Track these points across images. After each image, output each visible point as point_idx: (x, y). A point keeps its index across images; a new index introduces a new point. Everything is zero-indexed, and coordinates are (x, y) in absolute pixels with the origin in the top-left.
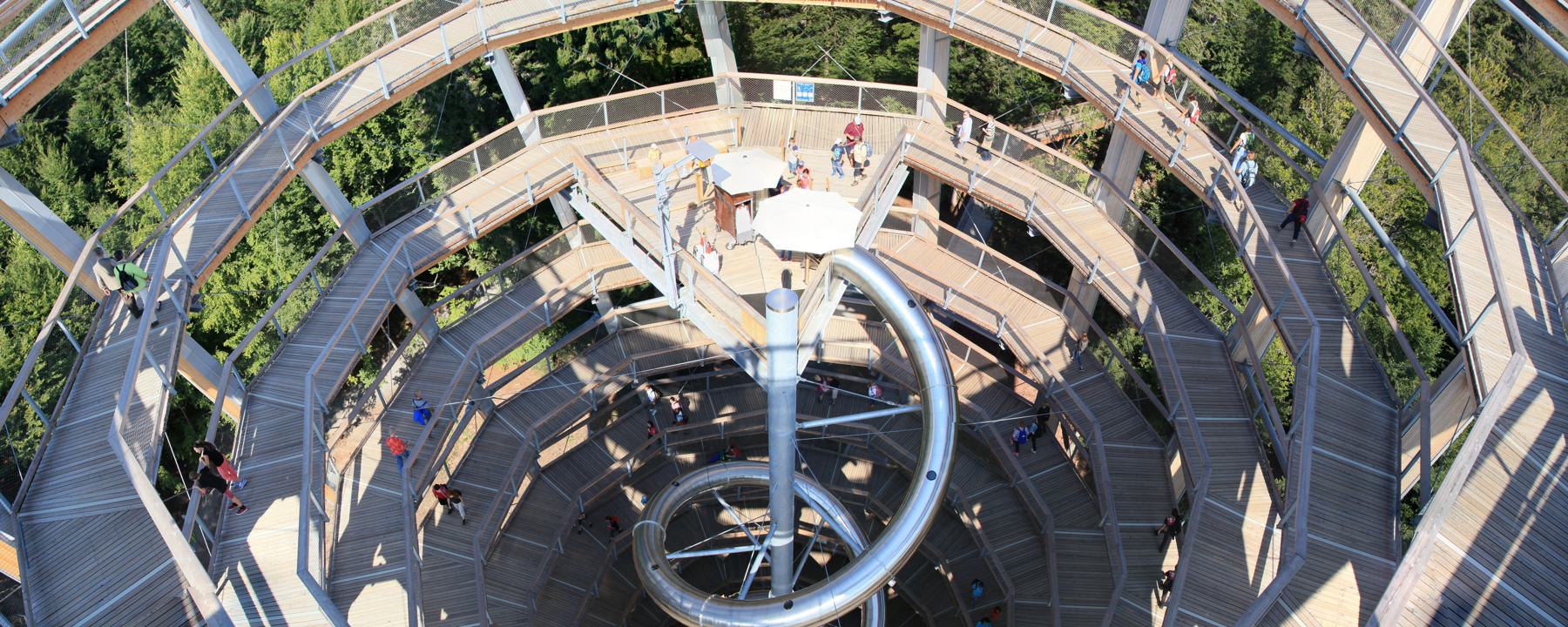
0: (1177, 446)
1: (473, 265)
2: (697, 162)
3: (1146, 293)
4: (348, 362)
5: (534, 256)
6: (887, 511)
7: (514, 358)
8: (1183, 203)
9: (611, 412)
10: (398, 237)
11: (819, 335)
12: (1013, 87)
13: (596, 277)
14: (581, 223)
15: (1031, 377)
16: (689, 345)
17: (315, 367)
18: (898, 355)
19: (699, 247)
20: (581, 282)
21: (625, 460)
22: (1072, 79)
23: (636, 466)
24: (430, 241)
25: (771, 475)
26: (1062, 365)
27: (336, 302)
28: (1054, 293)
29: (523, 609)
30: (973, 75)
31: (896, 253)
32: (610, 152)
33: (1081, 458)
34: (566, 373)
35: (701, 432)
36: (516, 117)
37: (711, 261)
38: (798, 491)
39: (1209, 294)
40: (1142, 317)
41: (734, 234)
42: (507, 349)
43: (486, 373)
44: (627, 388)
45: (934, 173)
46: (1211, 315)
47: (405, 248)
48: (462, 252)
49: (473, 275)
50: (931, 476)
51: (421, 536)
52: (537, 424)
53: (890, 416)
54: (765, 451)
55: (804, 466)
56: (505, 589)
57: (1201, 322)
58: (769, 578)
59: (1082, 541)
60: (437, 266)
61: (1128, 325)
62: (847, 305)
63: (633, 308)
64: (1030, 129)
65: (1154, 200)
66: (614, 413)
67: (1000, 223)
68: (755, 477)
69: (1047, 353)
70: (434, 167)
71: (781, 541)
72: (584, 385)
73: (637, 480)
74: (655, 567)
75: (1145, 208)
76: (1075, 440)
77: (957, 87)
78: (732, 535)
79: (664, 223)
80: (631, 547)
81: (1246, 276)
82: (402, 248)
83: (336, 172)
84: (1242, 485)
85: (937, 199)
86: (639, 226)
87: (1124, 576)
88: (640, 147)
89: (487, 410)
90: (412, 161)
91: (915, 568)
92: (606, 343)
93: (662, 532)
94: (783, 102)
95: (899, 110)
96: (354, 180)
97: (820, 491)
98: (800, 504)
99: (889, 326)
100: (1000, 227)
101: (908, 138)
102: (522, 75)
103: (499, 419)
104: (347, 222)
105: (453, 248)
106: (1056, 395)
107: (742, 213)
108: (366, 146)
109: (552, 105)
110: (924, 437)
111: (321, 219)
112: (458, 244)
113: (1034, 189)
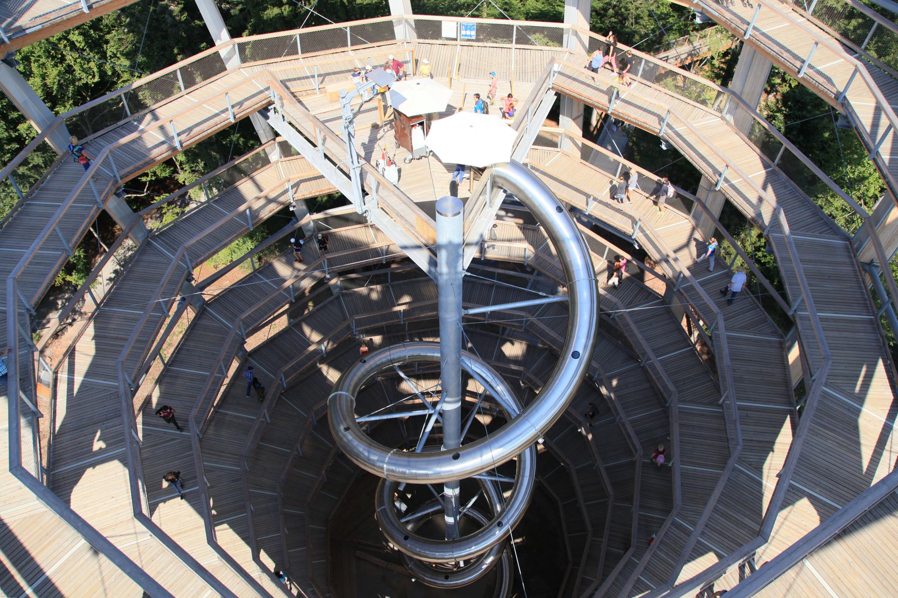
0: (797, 337)
2: (377, 87)
3: (770, 196)
4: (54, 264)
5: (236, 168)
6: (539, 383)
7: (223, 258)
8: (809, 112)
9: (307, 303)
10: (104, 147)
11: (482, 236)
12: (646, 18)
14: (278, 139)
15: (660, 272)
16: (376, 245)
17: (18, 270)
18: (550, 254)
19: (381, 161)
20: (280, 191)
21: (320, 342)
22: (703, 5)
23: (329, 347)
24: (136, 151)
25: (442, 353)
26: (689, 262)
27: (39, 206)
29: (237, 471)
30: (611, 11)
31: (545, 166)
32: (303, 78)
33: (704, 344)
34: (268, 270)
35: (384, 318)
36: (217, 43)
37: (391, 173)
38: (465, 366)
39: (832, 196)
40: (767, 219)
41: (411, 150)
42: (214, 250)
43: (196, 272)
44: (321, 282)
45: (578, 97)
46: (834, 218)
48: (169, 163)
50: (575, 355)
51: (139, 419)
53: (542, 305)
54: (436, 334)
55: (470, 345)
56: (221, 456)
57: (826, 223)
59: (703, 415)
60: (146, 175)
61: (752, 226)
62: (507, 211)
63: (326, 214)
65: (779, 111)
66: (310, 304)
69: (675, 251)
70: (137, 83)
71: (451, 406)
72: (285, 281)
73: (332, 359)
74: (347, 429)
75: (770, 118)
77: (597, 22)
78: (411, 402)
79: (350, 140)
80: (327, 414)
83: (36, 81)
84: (861, 379)
85: (581, 120)
86: (330, 143)
87: (739, 448)
88: (329, 74)
89: (198, 305)
93: (352, 400)
94: (447, 39)
95: (546, 44)
96: (58, 91)
97: (483, 365)
98: (466, 376)
99: (542, 228)
100: (633, 142)
101: (556, 67)
102: (223, 6)
104: (48, 129)
105: (159, 158)
106: (683, 288)
107: (417, 132)
108: (68, 58)
109: (250, 34)
110: (570, 322)
111: (22, 127)
112: (164, 156)
113: (667, 107)
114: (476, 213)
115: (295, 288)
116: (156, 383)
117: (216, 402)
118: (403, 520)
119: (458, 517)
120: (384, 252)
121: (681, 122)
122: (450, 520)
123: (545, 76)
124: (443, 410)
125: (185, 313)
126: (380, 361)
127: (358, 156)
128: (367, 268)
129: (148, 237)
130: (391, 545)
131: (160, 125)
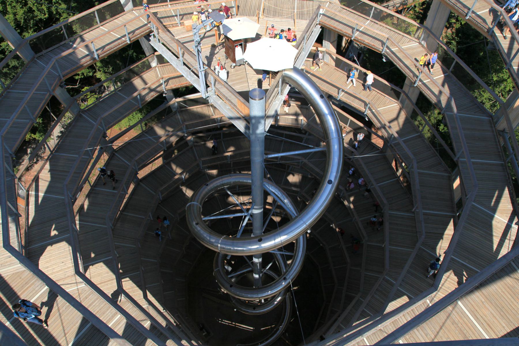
0: (459, 174)
1: (98, 75)
3: (446, 90)
7: (124, 124)
9: (174, 151)
10: (52, 58)
13: (165, 82)
14: (156, 53)
19: (217, 67)
20: (157, 84)
21: (181, 174)
23: (187, 176)
24: (73, 60)
25: (252, 180)
28: (395, 91)
33: (404, 177)
34: (150, 131)
37: (223, 75)
39: (483, 91)
40: (444, 103)
43: (108, 132)
44: (182, 139)
46: (484, 104)
47: (56, 64)
48: (92, 67)
49: (99, 80)
50: (330, 182)
51: (77, 218)
52: (137, 158)
53: (311, 153)
54: (249, 169)
55: (268, 176)
58: (251, 228)
60: (79, 75)
61: (435, 108)
64: (385, 4)
65: (453, 39)
66: (176, 151)
67: (367, 55)
68: (244, 181)
70: (71, 19)
71: (257, 211)
72: (160, 137)
73: (188, 184)
74: (197, 224)
75: (448, 43)
76: (402, 167)
78: (234, 208)
79: (199, 54)
80: (185, 215)
81: (510, 80)
82: (54, 64)
84: (495, 198)
85: (336, 43)
86: (187, 56)
87: (423, 237)
90: (60, 15)
91: (316, 226)
92: (172, 116)
93: (200, 208)
96: (24, 23)
98: (266, 194)
101: (321, 11)
103: (116, 156)
105: (85, 65)
106: (394, 144)
107: (238, 50)
112: (88, 63)
113: (387, 36)
114: (273, 98)
115: (167, 142)
116: (86, 197)
117: (121, 208)
118: (230, 276)
119: (261, 275)
120: (219, 121)
121: (395, 45)
122: (257, 276)
123: (315, 16)
124: (253, 214)
125: (102, 156)
126: (216, 185)
127: (204, 64)
128: (209, 130)
129: (80, 112)
130: (223, 290)
131: (86, 44)
